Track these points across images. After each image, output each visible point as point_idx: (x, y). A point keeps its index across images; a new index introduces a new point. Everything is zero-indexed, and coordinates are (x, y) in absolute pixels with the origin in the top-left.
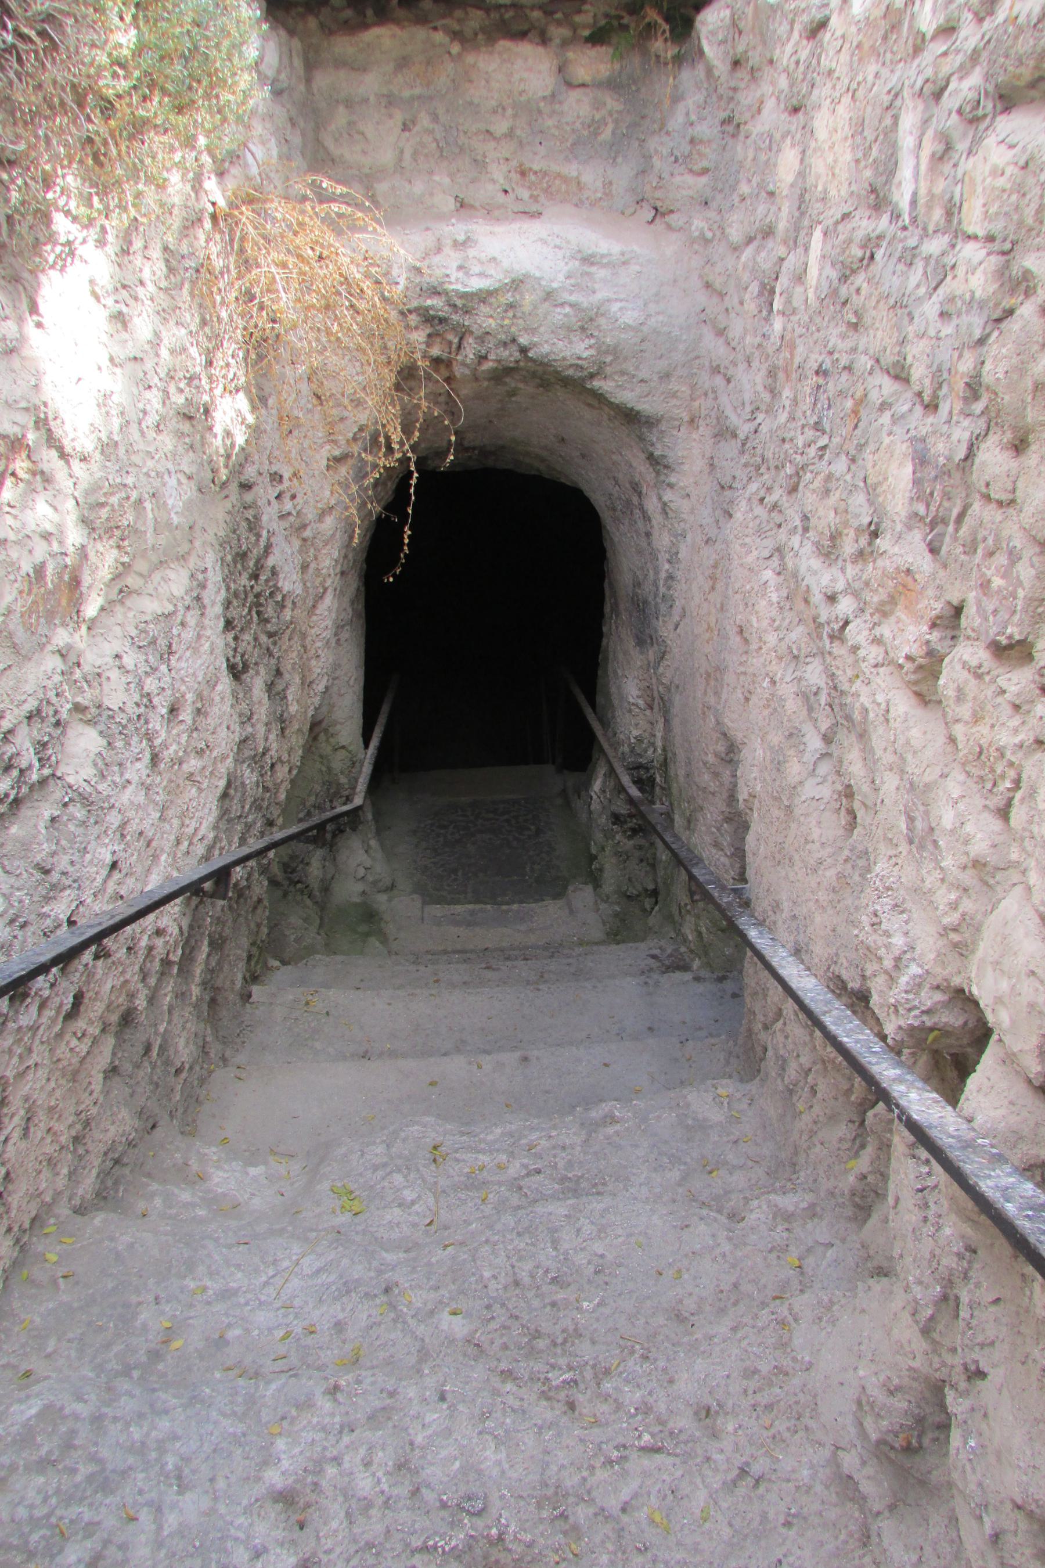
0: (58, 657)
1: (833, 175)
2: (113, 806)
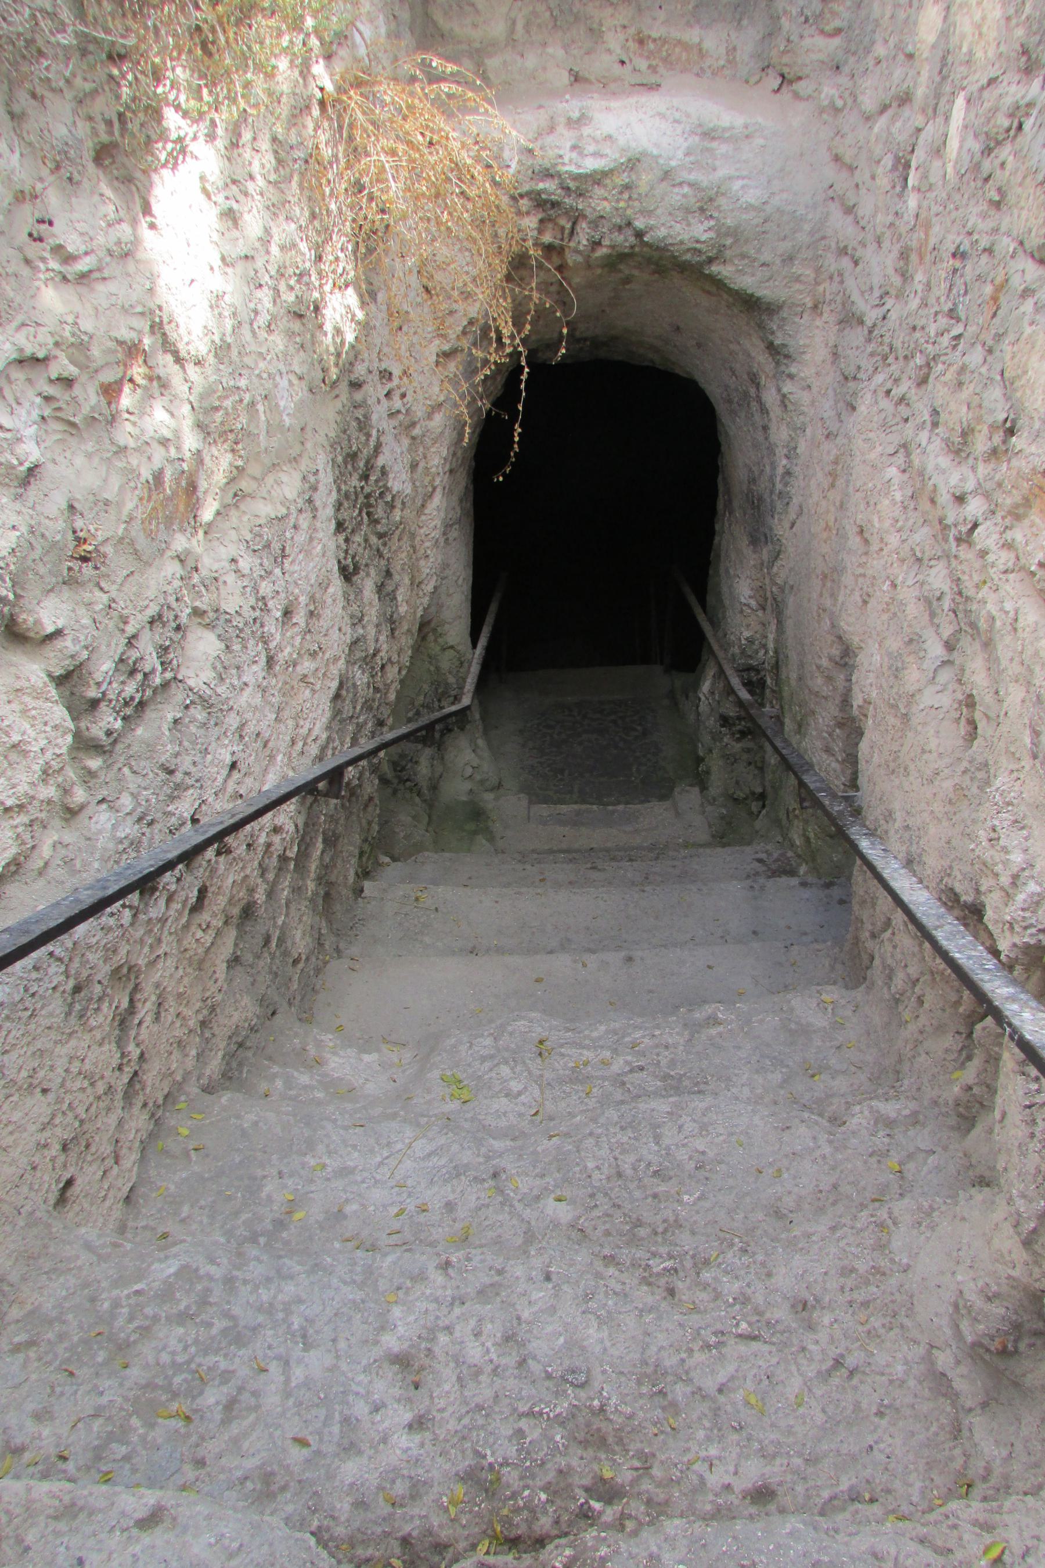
0: (177, 562)
1: (980, 34)
2: (232, 708)
